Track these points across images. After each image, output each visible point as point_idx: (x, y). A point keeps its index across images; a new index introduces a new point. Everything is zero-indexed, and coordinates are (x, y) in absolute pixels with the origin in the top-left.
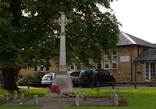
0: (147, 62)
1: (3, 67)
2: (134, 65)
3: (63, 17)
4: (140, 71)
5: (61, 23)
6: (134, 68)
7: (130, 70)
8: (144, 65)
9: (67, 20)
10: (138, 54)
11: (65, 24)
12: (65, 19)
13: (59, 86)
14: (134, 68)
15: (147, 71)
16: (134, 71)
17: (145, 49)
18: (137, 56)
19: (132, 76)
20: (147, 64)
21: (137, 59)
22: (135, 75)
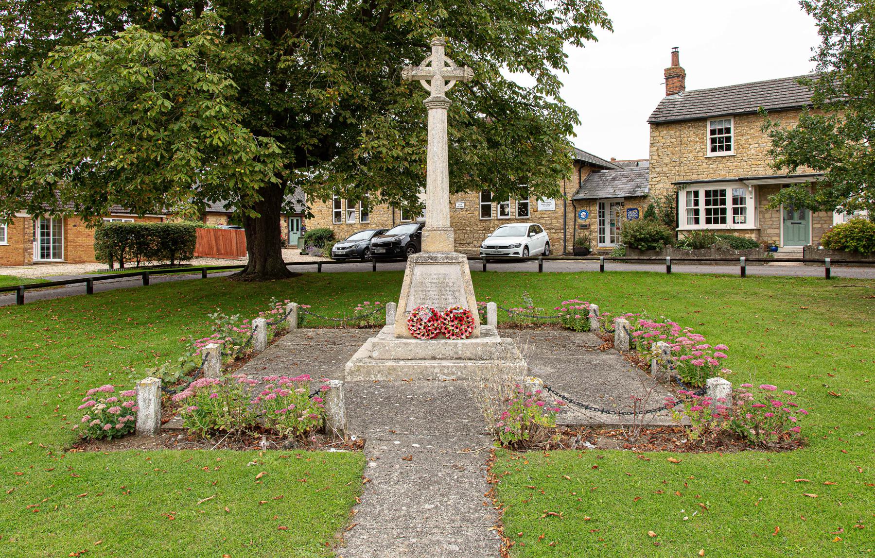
0: (602, 201)
1: (556, 13)
2: (570, 209)
3: (437, 55)
4: (587, 223)
5: (429, 82)
6: (571, 215)
7: (562, 221)
8: (595, 209)
9: (453, 70)
10: (580, 183)
11: (446, 83)
12: (447, 65)
13: (427, 311)
14: (571, 215)
15: (602, 223)
16: (570, 223)
17: (594, 172)
18: (577, 186)
19: (565, 235)
20: (602, 206)
21: (578, 192)
22: (572, 231)
